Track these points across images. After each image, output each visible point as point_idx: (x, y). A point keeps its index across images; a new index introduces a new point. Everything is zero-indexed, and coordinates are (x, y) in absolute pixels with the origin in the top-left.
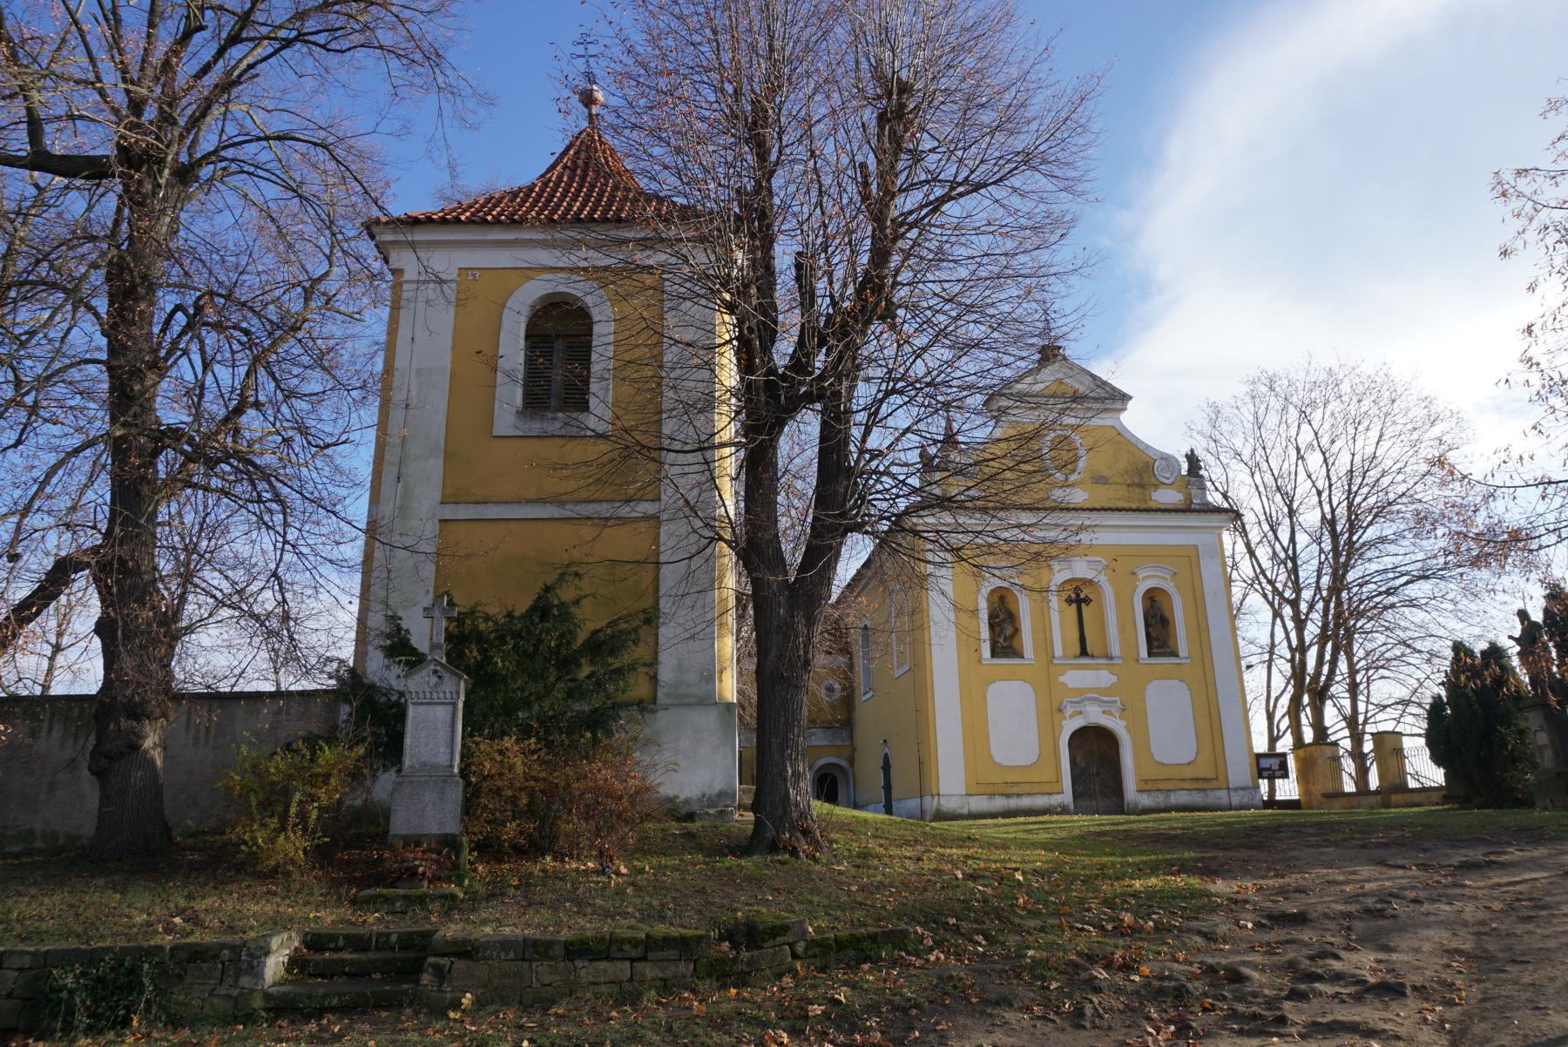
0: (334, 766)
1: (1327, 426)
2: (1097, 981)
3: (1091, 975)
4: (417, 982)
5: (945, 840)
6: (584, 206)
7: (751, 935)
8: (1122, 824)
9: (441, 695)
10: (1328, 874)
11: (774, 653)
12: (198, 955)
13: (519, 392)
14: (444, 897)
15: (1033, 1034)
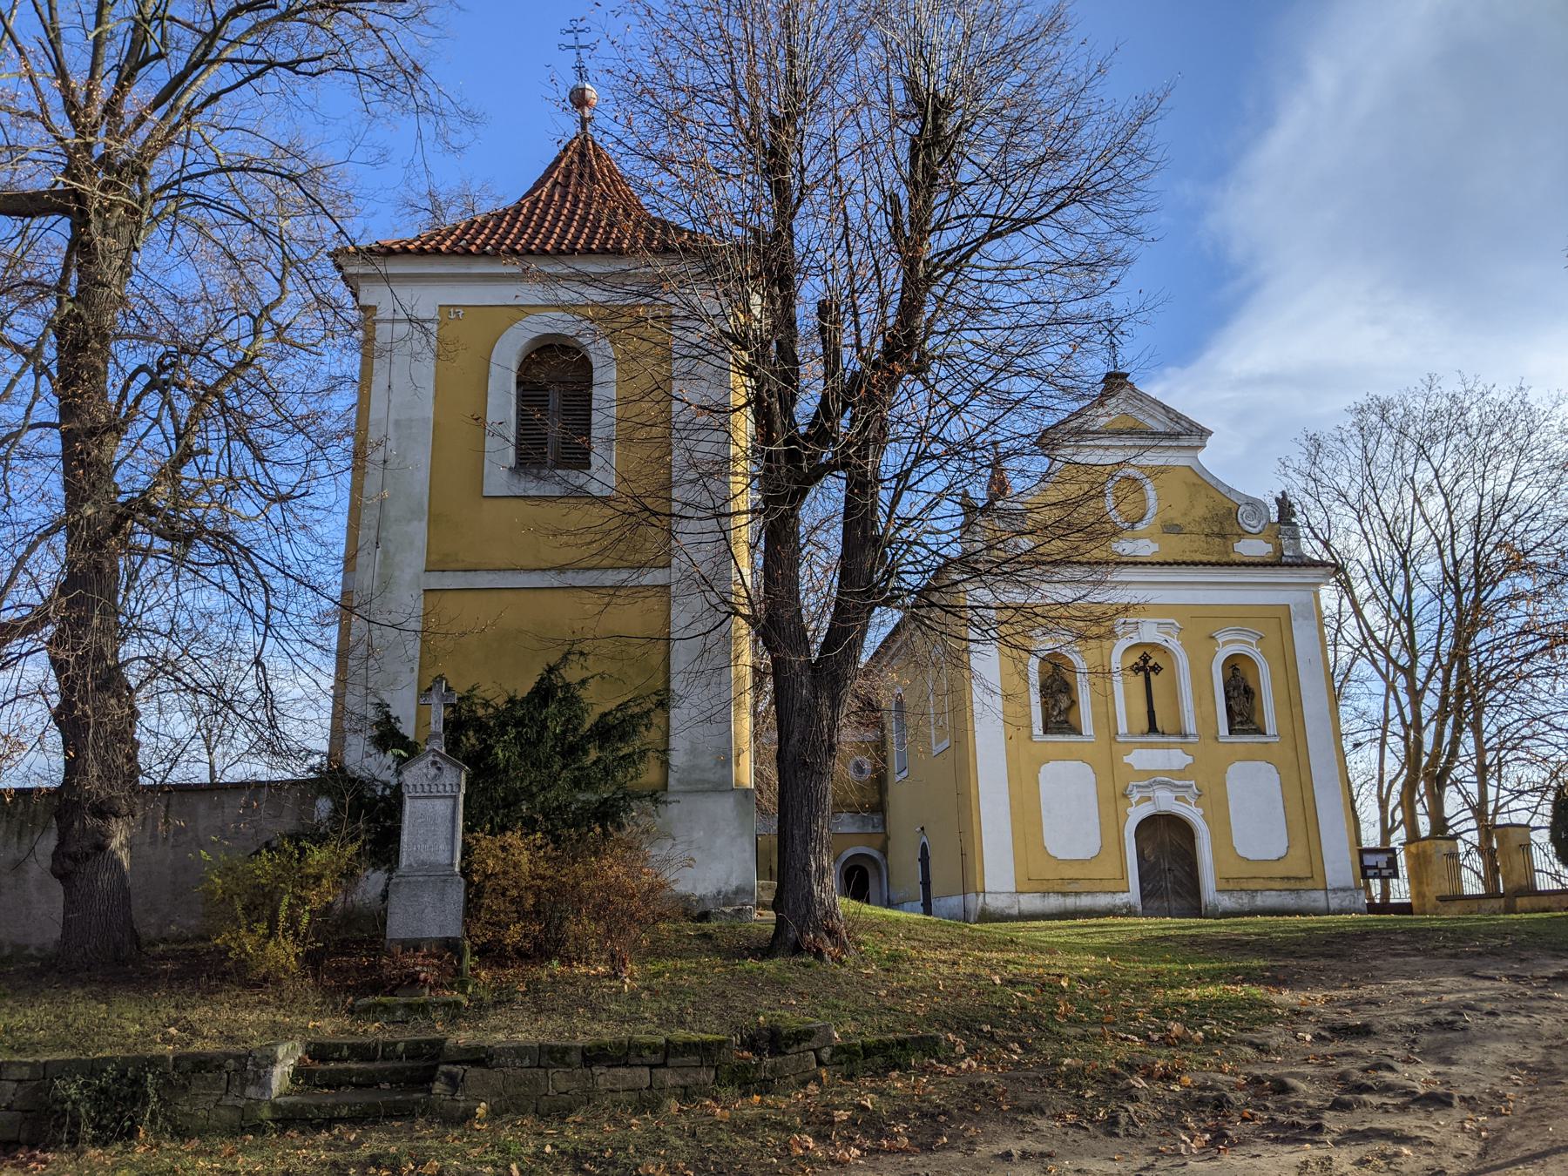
0: (325, 866)
1: (1448, 464)
2: (1134, 1090)
3: (1128, 1083)
4: (429, 1091)
5: (985, 943)
6: (579, 232)
7: (776, 1041)
8: (1191, 928)
9: (441, 788)
10: (1406, 986)
11: (796, 736)
12: (202, 1064)
13: (512, 452)
14: (447, 1004)
15: (1064, 1141)
